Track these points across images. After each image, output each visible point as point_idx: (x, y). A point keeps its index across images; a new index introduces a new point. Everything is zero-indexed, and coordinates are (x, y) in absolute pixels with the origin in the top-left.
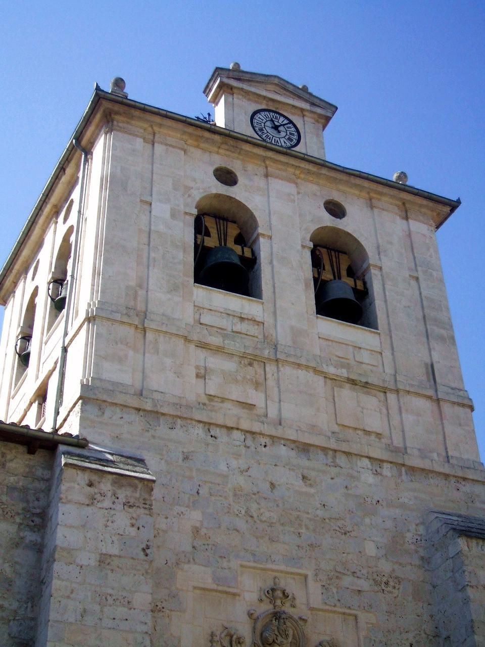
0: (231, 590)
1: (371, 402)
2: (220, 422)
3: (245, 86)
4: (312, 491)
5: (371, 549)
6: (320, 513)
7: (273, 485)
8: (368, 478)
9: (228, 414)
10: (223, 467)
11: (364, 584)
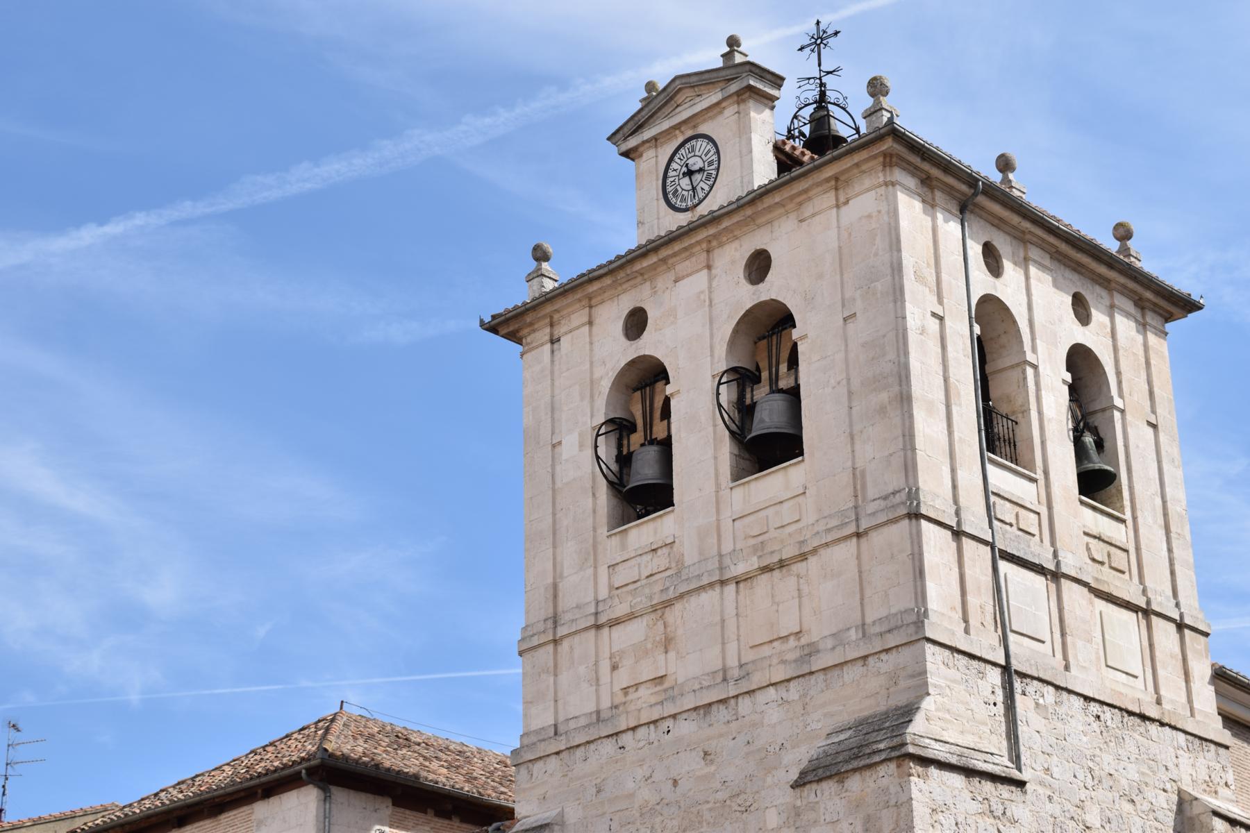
1: (784, 584)
2: (623, 727)
3: (647, 134)
4: (713, 768)
6: (720, 796)
7: (675, 782)
8: (774, 715)
9: (645, 703)
10: (630, 785)
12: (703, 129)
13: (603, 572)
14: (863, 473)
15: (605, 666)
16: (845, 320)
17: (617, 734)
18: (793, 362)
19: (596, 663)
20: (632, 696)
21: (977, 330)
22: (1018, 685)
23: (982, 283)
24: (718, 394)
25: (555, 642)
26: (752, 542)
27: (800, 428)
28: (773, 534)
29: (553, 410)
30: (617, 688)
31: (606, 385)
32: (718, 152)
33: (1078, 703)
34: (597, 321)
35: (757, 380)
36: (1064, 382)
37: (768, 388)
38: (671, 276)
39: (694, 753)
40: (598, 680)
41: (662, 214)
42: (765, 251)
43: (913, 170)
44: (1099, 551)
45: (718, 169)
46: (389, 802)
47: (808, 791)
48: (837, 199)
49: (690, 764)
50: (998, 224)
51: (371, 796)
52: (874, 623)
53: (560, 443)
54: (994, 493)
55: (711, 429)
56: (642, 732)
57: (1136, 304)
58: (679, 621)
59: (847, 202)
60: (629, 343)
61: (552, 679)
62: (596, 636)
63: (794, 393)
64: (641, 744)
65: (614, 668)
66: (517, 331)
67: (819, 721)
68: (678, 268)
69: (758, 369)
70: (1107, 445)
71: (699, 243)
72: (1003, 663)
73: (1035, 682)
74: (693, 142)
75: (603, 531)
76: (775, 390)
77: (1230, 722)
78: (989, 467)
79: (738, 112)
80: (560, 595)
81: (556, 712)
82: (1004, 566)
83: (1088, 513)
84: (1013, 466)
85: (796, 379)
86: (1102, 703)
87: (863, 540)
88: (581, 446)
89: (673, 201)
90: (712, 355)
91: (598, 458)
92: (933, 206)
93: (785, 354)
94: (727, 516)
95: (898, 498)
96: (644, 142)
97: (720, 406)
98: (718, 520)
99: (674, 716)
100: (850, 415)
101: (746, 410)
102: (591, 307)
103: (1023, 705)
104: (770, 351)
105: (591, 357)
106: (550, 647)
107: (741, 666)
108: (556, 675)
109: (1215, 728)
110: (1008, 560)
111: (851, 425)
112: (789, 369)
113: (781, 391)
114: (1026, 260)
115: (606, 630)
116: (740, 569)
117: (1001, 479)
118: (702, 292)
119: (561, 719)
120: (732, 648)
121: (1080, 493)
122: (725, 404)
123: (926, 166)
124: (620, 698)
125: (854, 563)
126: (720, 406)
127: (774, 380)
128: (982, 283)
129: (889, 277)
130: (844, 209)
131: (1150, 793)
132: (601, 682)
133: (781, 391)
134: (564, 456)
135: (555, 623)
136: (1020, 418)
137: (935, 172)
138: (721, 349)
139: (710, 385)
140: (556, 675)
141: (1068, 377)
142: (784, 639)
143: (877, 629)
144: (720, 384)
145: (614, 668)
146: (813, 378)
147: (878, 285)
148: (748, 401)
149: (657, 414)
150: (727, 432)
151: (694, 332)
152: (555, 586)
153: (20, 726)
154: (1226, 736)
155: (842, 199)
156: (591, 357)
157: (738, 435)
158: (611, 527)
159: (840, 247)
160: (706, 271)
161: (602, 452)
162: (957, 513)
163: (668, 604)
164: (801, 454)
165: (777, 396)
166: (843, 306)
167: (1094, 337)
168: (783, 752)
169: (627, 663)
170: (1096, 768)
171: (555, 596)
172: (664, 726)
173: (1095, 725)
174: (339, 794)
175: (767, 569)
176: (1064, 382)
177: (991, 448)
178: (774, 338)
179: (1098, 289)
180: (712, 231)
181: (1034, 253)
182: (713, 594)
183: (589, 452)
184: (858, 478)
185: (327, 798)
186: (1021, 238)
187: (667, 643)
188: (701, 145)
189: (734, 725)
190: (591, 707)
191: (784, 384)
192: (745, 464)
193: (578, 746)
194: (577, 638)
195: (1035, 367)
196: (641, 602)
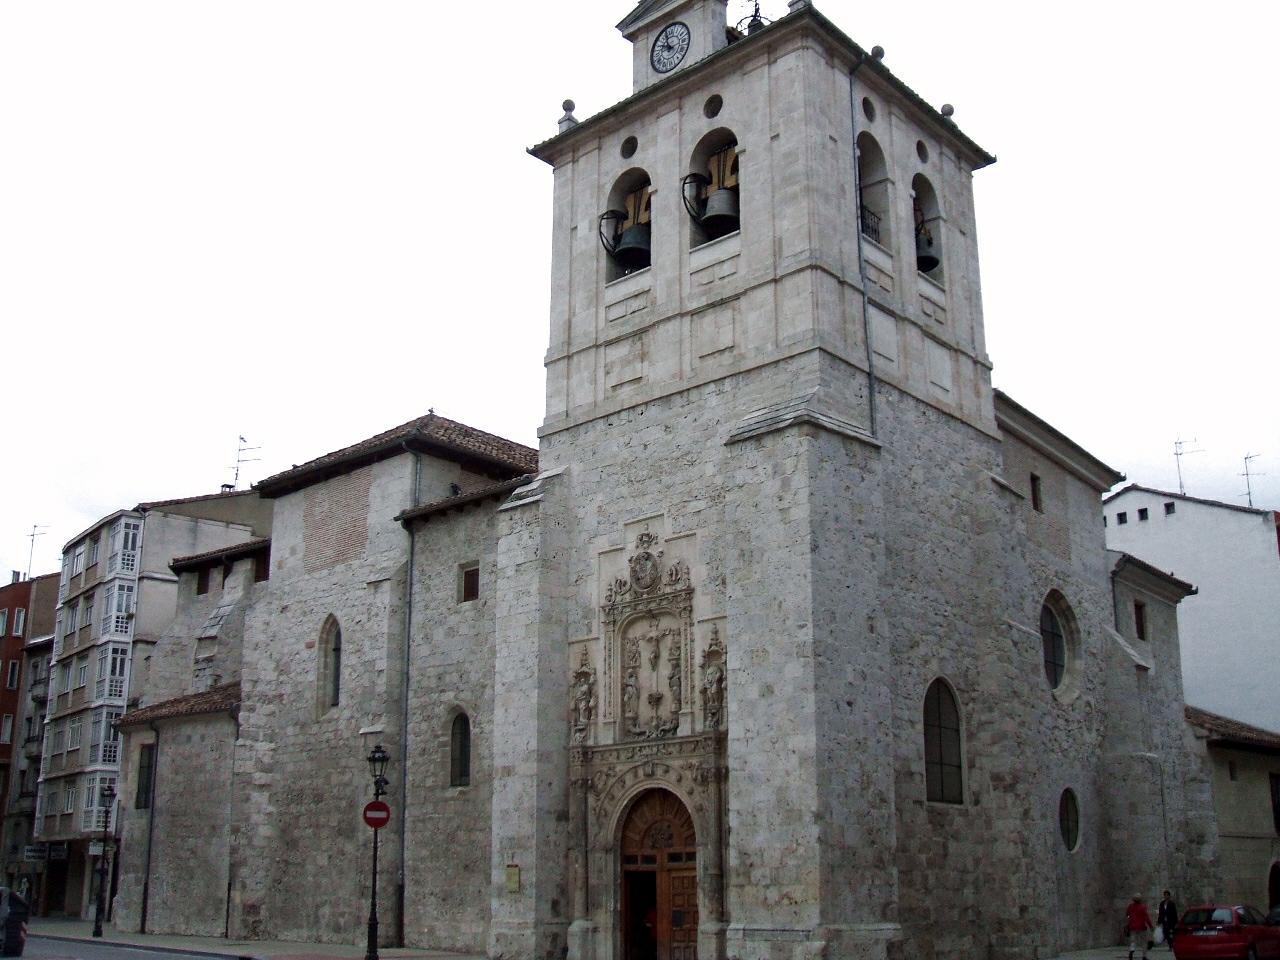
0: (619, 547)
1: (725, 315)
3: (641, 24)
4: (670, 437)
5: (710, 470)
9: (627, 396)
11: (701, 505)
12: (679, 19)
13: (602, 311)
14: (780, 239)
15: (601, 373)
16: (772, 138)
17: (607, 416)
18: (735, 169)
19: (595, 370)
20: (619, 391)
21: (858, 153)
22: (876, 387)
23: (862, 123)
24: (683, 190)
25: (569, 357)
26: (703, 288)
27: (738, 211)
28: (718, 282)
29: (572, 206)
30: (609, 386)
31: (608, 188)
32: (689, 33)
33: (912, 403)
34: (604, 147)
35: (710, 182)
36: (911, 196)
37: (717, 187)
38: (655, 115)
39: (659, 427)
40: (596, 381)
41: (650, 75)
42: (709, 118)
43: (821, 42)
44: (929, 309)
45: (688, 44)
46: (459, 467)
47: (736, 450)
48: (769, 59)
49: (655, 434)
50: (873, 87)
51: (448, 463)
52: (784, 339)
53: (576, 228)
54: (866, 261)
55: (677, 213)
56: (624, 415)
57: (955, 155)
58: (652, 342)
59: (775, 61)
60: (624, 160)
61: (565, 382)
62: (596, 354)
63: (735, 191)
64: (624, 422)
65: (607, 373)
66: (552, 155)
67: (744, 404)
68: (659, 109)
69: (711, 176)
70: (934, 242)
71: (674, 92)
72: (868, 371)
73: (887, 386)
74: (672, 28)
75: (603, 284)
76: (721, 187)
77: (1001, 426)
78: (862, 241)
79: (703, 6)
80: (573, 326)
81: (568, 402)
82: (872, 311)
83: (920, 280)
84: (874, 242)
85: (737, 180)
86: (927, 404)
87: (779, 286)
88: (590, 229)
89: (658, 66)
90: (680, 165)
91: (601, 233)
92: (833, 67)
93: (730, 163)
94: (687, 270)
95: (803, 257)
96: (639, 29)
97: (684, 198)
98: (680, 275)
99: (646, 403)
100: (773, 201)
101: (701, 202)
102: (600, 138)
103: (880, 399)
104: (719, 161)
105: (599, 170)
106: (566, 360)
107: (692, 370)
108: (568, 378)
109: (993, 430)
110: (873, 305)
111: (773, 208)
112: (732, 174)
113: (725, 188)
114: (890, 113)
115: (602, 349)
116: (694, 305)
117: (870, 252)
118: (676, 124)
119: (571, 405)
120: (687, 358)
121: (919, 269)
122: (688, 198)
123: (829, 39)
124: (610, 394)
125: (772, 299)
126: (684, 198)
127: (721, 182)
128: (862, 123)
129: (803, 110)
130: (773, 67)
131: (953, 465)
132: (598, 382)
133: (725, 188)
134: (579, 236)
135: (569, 344)
136: (882, 216)
137: (836, 44)
138: (687, 161)
139: (677, 184)
140: (568, 378)
141: (913, 193)
142: (721, 351)
143: (787, 343)
144: (685, 183)
145: (607, 373)
146: (750, 179)
147: (795, 115)
148: (703, 197)
149: (643, 207)
150: (689, 216)
151: (667, 152)
152: (570, 321)
153: (238, 439)
154: (999, 435)
155: (772, 59)
156: (599, 170)
157: (695, 219)
158: (609, 280)
159: (770, 91)
160: (678, 110)
161: (604, 230)
162: (842, 270)
163: (644, 330)
164: (739, 229)
165: (722, 191)
166: (771, 130)
167: (926, 170)
168: (718, 426)
169: (616, 369)
170: (922, 445)
171: (570, 327)
172: (639, 410)
173: (922, 419)
174: (426, 459)
175: (712, 305)
176: (911, 196)
177: (863, 231)
178: (722, 155)
179: (933, 142)
180: (683, 84)
181: (895, 110)
182: (676, 323)
183: (595, 232)
184: (778, 246)
185: (418, 461)
186: (887, 99)
187: (643, 357)
188: (678, 29)
189: (686, 408)
190: (591, 399)
191: (729, 183)
192: (698, 238)
193: (582, 424)
194: (583, 355)
195: (893, 183)
196: (628, 329)
